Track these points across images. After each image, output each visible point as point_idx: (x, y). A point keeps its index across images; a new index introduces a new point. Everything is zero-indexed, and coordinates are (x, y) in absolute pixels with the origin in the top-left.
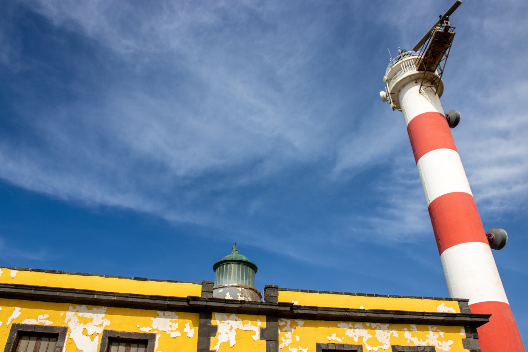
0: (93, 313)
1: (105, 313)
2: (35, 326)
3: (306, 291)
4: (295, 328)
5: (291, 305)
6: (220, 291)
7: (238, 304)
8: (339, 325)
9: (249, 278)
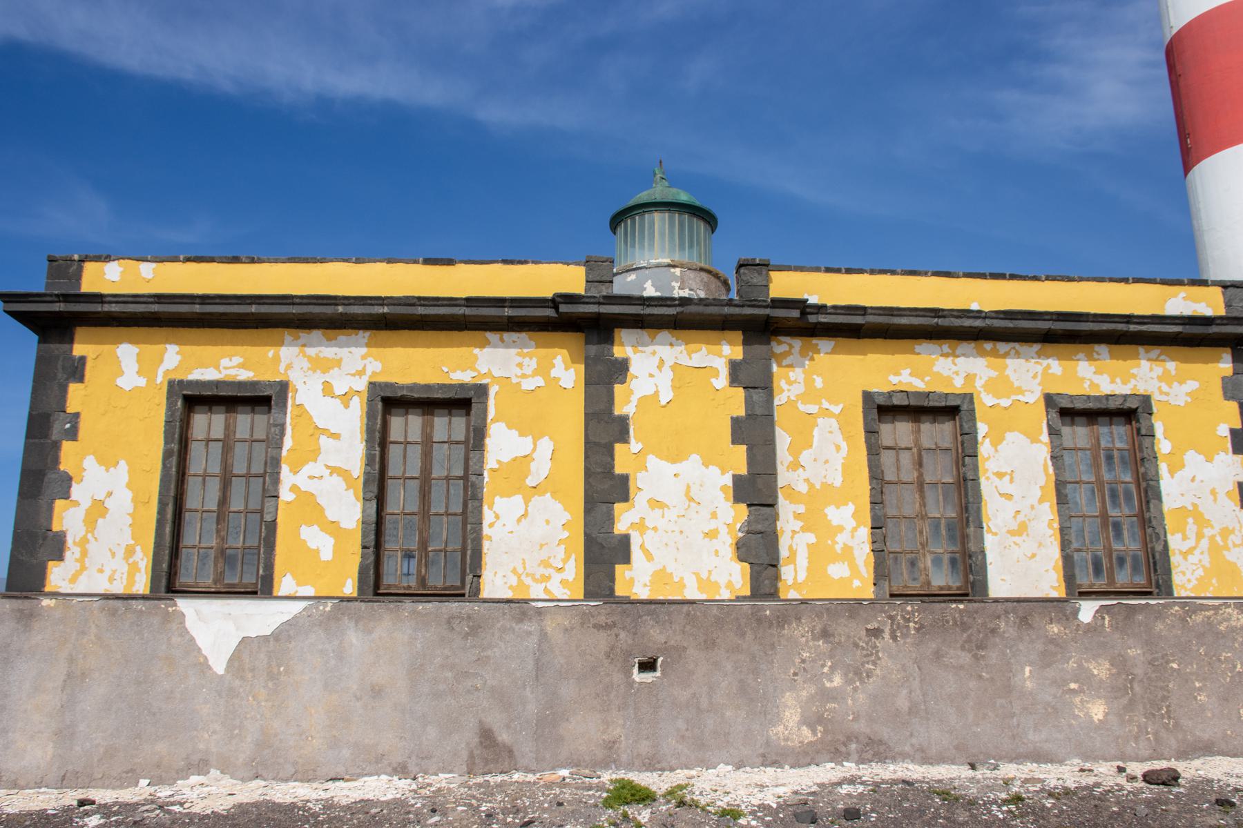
0: (341, 347)
1: (367, 345)
2: (217, 384)
3: (838, 271)
4: (812, 359)
5: (801, 304)
6: (629, 279)
7: (675, 306)
8: (918, 348)
9: (699, 244)
